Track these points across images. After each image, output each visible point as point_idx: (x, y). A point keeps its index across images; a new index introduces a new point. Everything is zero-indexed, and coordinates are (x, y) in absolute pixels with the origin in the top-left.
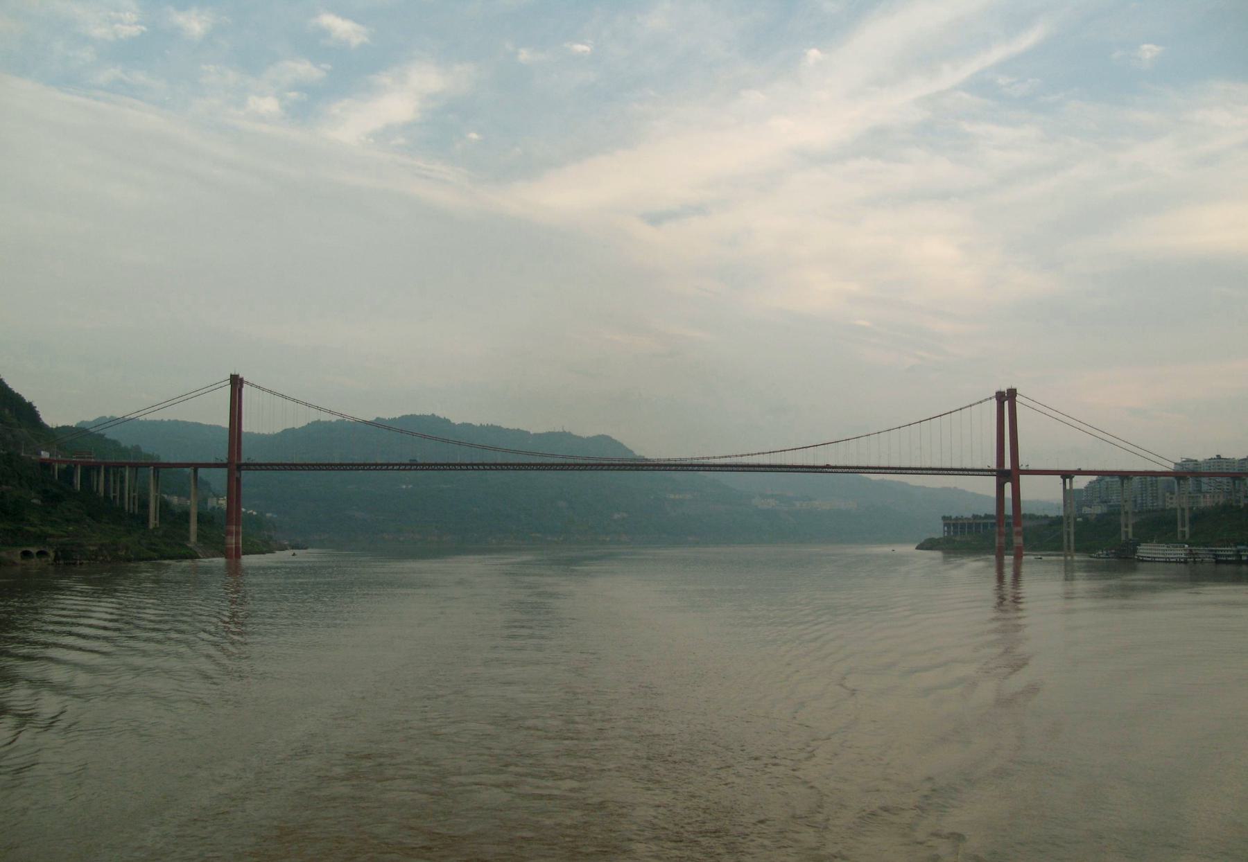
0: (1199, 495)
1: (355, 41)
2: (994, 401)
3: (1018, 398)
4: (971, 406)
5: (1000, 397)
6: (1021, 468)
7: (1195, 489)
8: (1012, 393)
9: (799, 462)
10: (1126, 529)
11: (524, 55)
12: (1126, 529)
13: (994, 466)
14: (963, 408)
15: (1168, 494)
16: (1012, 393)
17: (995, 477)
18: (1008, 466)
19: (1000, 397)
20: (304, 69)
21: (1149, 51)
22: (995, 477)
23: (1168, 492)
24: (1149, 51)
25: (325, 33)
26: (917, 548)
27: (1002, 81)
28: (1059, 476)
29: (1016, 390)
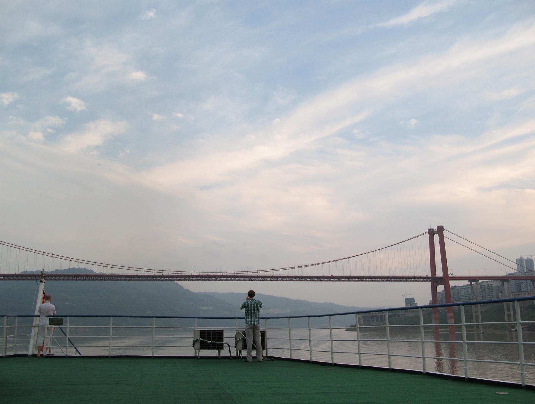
0: (520, 293)
1: (79, 109)
2: (427, 236)
3: (444, 232)
4: (316, 264)
5: (431, 232)
6: (450, 276)
7: (517, 290)
8: (441, 229)
9: (300, 274)
10: (509, 313)
11: (156, 117)
12: (509, 313)
13: (429, 275)
14: (331, 262)
15: (500, 294)
16: (441, 229)
17: (431, 282)
18: (439, 273)
19: (431, 232)
20: (55, 120)
21: (414, 122)
22: (431, 282)
23: (500, 293)
24: (414, 122)
25: (69, 104)
26: (346, 331)
27: (355, 131)
28: (468, 281)
29: (443, 226)
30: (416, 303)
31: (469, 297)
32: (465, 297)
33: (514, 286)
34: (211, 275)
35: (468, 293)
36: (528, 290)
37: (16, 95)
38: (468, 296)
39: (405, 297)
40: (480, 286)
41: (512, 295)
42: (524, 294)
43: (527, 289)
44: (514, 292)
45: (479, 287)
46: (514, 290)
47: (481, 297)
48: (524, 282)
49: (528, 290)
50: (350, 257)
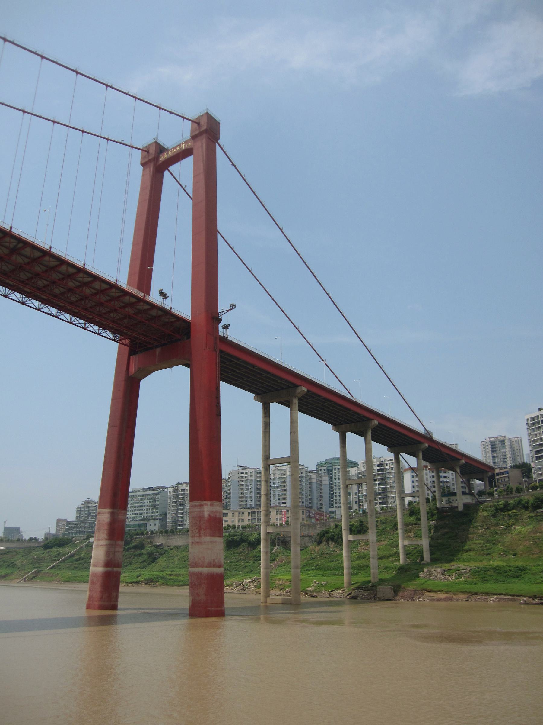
12: (245, 473)
30: (22, 535)
31: (143, 516)
32: (135, 514)
33: (253, 495)
34: (67, 261)
35: (141, 506)
36: (285, 503)
37: (160, 162)
38: (141, 514)
39: (5, 524)
40: (174, 491)
41: (249, 513)
42: (277, 512)
43: (285, 493)
44: (253, 508)
45: (172, 493)
46: (253, 503)
47: (173, 515)
48: (278, 486)
49: (285, 503)
50: (235, 166)
